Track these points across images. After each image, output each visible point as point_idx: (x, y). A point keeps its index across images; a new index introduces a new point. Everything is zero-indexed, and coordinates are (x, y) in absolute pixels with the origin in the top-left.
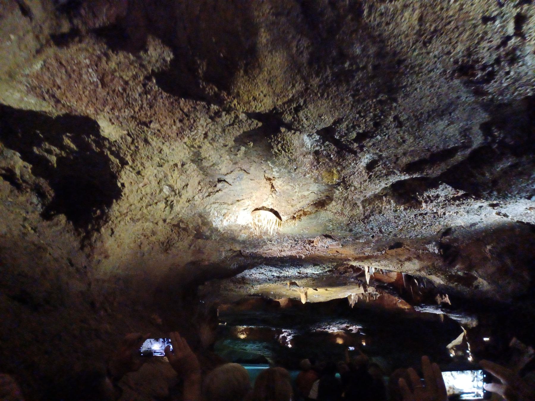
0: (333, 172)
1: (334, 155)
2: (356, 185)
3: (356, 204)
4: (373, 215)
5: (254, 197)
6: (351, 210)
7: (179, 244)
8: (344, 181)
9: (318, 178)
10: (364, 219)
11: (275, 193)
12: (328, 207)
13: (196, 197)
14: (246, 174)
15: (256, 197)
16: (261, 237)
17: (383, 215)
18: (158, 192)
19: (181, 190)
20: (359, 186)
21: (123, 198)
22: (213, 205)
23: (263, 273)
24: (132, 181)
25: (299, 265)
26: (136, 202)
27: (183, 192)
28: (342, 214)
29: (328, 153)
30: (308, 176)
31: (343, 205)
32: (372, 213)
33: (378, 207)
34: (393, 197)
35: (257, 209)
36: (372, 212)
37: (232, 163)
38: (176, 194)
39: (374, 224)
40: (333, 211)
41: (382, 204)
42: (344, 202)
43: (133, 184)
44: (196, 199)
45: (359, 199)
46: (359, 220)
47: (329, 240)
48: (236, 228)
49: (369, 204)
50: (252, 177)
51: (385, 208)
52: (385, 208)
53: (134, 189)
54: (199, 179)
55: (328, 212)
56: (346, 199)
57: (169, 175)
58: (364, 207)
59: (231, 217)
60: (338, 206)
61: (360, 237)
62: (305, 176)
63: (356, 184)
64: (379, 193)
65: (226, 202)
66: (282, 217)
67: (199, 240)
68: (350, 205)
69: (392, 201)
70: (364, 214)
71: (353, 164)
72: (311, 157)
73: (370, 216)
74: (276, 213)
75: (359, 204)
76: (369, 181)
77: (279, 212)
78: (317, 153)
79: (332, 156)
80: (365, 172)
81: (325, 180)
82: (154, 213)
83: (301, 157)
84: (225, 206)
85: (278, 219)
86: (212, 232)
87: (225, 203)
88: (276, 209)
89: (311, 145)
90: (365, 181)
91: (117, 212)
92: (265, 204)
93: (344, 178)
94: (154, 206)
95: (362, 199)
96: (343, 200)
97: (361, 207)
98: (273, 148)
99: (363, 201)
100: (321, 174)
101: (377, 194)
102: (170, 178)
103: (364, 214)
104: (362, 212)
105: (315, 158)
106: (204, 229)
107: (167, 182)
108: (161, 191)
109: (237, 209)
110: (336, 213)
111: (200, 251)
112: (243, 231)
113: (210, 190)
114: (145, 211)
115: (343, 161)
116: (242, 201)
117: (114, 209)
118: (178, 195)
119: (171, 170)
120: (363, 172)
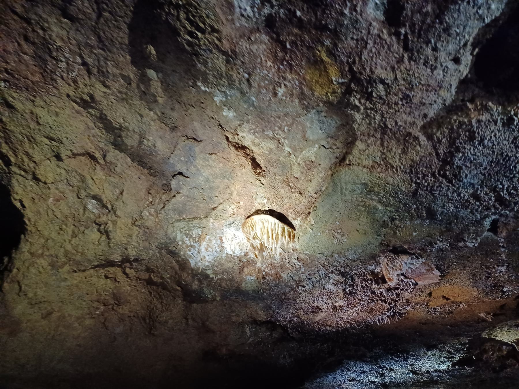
0: (322, 60)
1: (302, 10)
2: (383, 76)
3: (409, 134)
4: (458, 150)
5: (235, 193)
6: (404, 152)
7: (165, 316)
8: (355, 77)
9: (302, 93)
10: (442, 168)
11: (264, 176)
12: (351, 157)
13: (146, 213)
14: (196, 143)
15: (239, 194)
16: (278, 276)
17: (481, 142)
18: (81, 211)
19: (114, 202)
20: (391, 76)
21: (29, 228)
22: (176, 225)
23: (354, 380)
24: (34, 196)
25: (402, 352)
26: (54, 235)
27: (118, 204)
28: (388, 166)
29: (289, 10)
30: (281, 91)
31: (382, 145)
32: (454, 147)
33: (461, 124)
34: (490, 95)
35: (249, 217)
36: (452, 142)
37: (168, 128)
38: (110, 211)
39: (471, 176)
40: (365, 163)
41: (467, 115)
42: (382, 139)
43: (36, 201)
44: (146, 218)
45: (413, 124)
46: (433, 175)
47: (405, 258)
48: (231, 265)
49: (439, 127)
50: (210, 149)
51: (479, 121)
52: (479, 121)
53: (41, 210)
54: (146, 185)
55: (355, 167)
56: (384, 129)
57: (88, 177)
58: (430, 137)
59: (210, 240)
60: (371, 148)
61: (462, 232)
62: (275, 94)
63: (380, 72)
64: (454, 101)
65: (197, 215)
66: (294, 222)
67: (195, 305)
68: (398, 141)
69: (490, 104)
70: (437, 154)
71: (347, 12)
72: (265, 38)
73: (452, 155)
74: (282, 218)
75: (416, 132)
76: (410, 59)
77: (284, 213)
78: (270, 23)
79: (298, 13)
80: (390, 34)
81: (319, 92)
82: (84, 250)
83: (244, 44)
84: (196, 222)
85: (286, 227)
86: (200, 281)
87: (195, 218)
88: (279, 210)
89: (252, 7)
90: (400, 61)
91: (27, 254)
92: (260, 207)
93: (351, 70)
94: (80, 236)
95: (420, 123)
96: (378, 135)
97: (423, 139)
98: (179, 35)
99: (424, 127)
100: (304, 79)
101: (451, 106)
102: (90, 182)
103: (437, 154)
104: (430, 149)
105: (272, 38)
106: (186, 277)
107: (89, 191)
108: (85, 208)
109: (216, 224)
110: (373, 167)
111: (204, 329)
112: (246, 271)
113: (164, 197)
114: (69, 247)
115: (324, 12)
116: (220, 207)
117: (23, 250)
118: (112, 212)
119: (91, 171)
120: (386, 36)
